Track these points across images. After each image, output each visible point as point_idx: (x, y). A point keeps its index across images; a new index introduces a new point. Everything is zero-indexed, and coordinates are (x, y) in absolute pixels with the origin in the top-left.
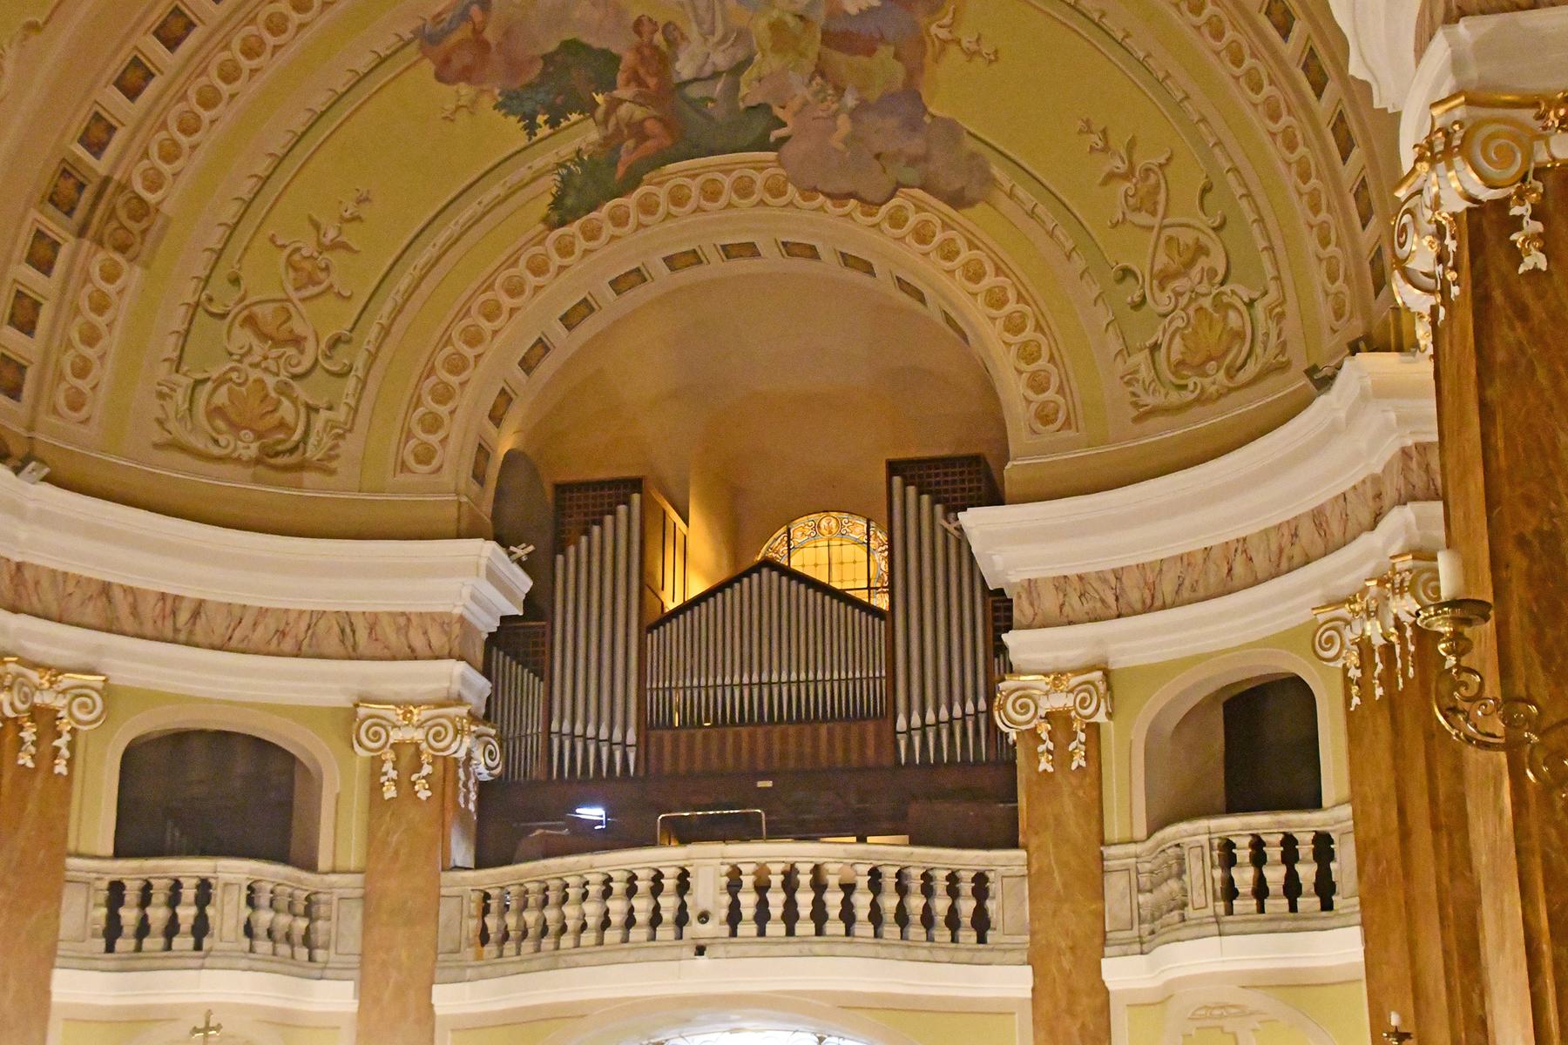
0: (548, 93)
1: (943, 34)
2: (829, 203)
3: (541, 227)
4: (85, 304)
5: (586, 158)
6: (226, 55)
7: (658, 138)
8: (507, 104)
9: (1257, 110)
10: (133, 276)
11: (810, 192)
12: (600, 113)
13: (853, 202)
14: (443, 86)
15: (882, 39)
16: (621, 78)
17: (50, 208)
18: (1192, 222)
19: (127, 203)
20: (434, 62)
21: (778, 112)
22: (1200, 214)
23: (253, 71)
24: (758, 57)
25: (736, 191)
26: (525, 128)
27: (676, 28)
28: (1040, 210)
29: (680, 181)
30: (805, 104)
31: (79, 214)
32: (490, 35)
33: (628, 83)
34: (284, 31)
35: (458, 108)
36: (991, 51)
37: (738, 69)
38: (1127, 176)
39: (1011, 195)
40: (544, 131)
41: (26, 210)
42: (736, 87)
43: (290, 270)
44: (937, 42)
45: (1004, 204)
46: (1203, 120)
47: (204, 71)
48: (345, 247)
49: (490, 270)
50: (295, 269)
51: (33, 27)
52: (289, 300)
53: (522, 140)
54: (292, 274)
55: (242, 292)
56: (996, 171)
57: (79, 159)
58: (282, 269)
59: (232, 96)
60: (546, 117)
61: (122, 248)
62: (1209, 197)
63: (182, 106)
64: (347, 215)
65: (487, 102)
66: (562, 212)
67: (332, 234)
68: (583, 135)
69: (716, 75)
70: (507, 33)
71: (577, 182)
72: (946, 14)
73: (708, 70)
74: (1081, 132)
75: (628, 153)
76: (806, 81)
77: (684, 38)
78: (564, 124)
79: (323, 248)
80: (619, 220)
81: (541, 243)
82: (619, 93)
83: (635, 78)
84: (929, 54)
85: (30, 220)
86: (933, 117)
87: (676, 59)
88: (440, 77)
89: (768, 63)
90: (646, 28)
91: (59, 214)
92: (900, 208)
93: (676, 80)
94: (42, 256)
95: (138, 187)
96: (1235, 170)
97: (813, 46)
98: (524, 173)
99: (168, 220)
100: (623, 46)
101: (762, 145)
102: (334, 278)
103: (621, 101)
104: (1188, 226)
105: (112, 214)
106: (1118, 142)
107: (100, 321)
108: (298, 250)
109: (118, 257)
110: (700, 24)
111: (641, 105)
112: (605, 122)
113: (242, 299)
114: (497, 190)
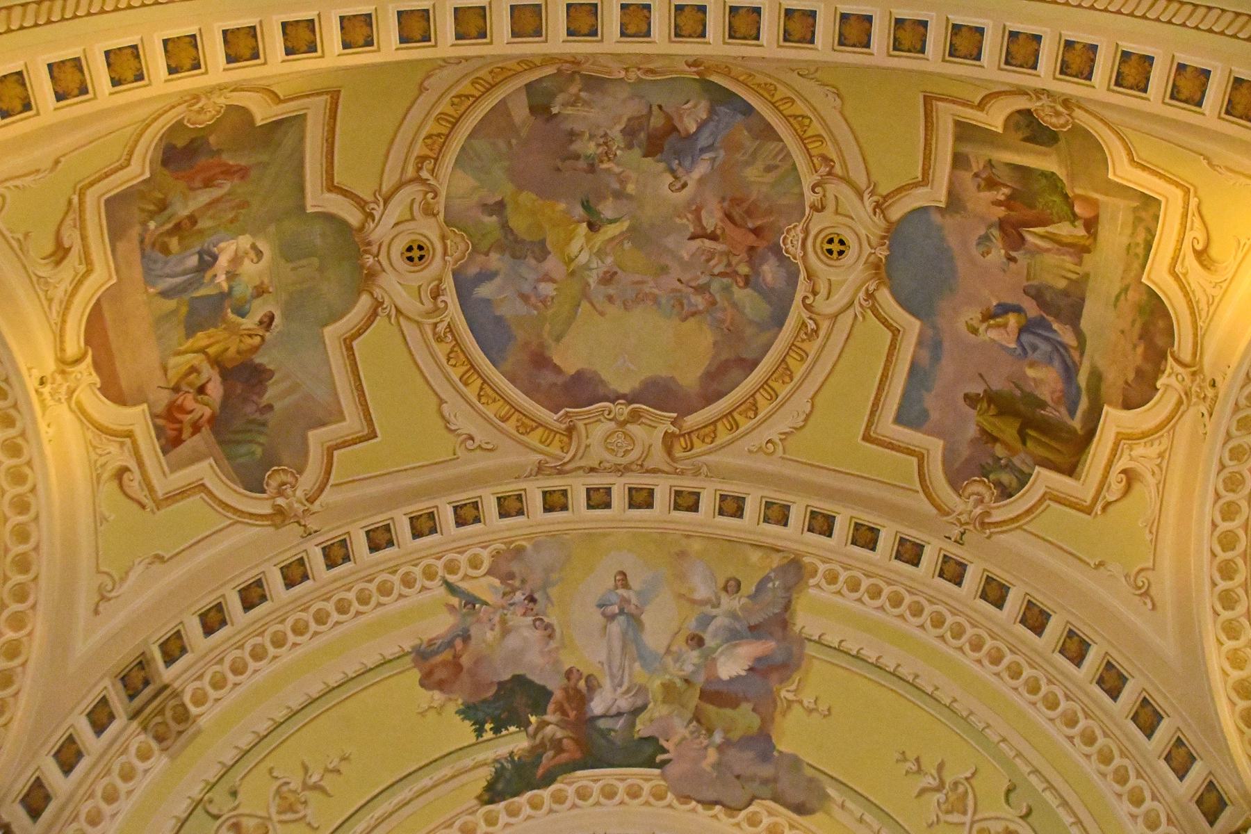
0: (496, 709)
1: (790, 696)
2: (700, 807)
3: (475, 802)
4: (116, 768)
5: (516, 758)
6: (280, 627)
7: (571, 750)
8: (468, 712)
9: (1054, 724)
10: (160, 762)
11: (685, 798)
12: (531, 729)
13: (718, 808)
14: (423, 690)
15: (746, 699)
16: (551, 707)
17: (120, 686)
18: (999, 814)
19: (175, 707)
20: (420, 671)
21: (662, 742)
22: (1006, 807)
23: (295, 645)
24: (651, 706)
25: (628, 794)
26: (475, 730)
27: (596, 678)
28: (867, 817)
29: (585, 783)
30: (684, 739)
31: (138, 702)
32: (465, 661)
33: (554, 712)
34: (324, 624)
35: (431, 707)
36: (826, 708)
37: (636, 712)
38: (940, 788)
39: (843, 806)
40: (489, 735)
41: (102, 678)
42: (633, 725)
43: (277, 798)
44: (784, 701)
45: (836, 811)
46: (1004, 740)
47: (261, 634)
48: (322, 790)
49: (453, 813)
50: (283, 798)
51: (160, 558)
52: (270, 819)
53: (474, 740)
54: (277, 800)
55: (237, 803)
56: (830, 791)
57: (153, 659)
58: (271, 795)
59: (275, 657)
60: (492, 725)
61: (160, 739)
62: (1012, 796)
63: (238, 653)
64: (331, 767)
65: (452, 708)
66: (493, 793)
67: (315, 778)
68: (516, 742)
69: (619, 714)
70: (476, 663)
71: (507, 775)
72: (793, 682)
73: (614, 711)
74: (898, 761)
75: (548, 758)
76: (685, 723)
77: (600, 686)
78: (504, 732)
79: (306, 786)
80: (535, 805)
81: (474, 813)
82: (548, 718)
83: (561, 709)
84: (779, 709)
85: (100, 687)
86: (780, 752)
87: (592, 699)
88: (422, 685)
89: (658, 710)
90: (575, 676)
91: (123, 694)
92: (755, 813)
93: (589, 715)
94: (100, 718)
95: (187, 699)
96: (1036, 771)
97: (693, 700)
98: (469, 762)
99: (199, 732)
100: (555, 685)
101: (650, 763)
102: (309, 811)
103: (548, 724)
104: (997, 818)
105: (161, 712)
106: (930, 766)
107: (123, 787)
108: (287, 783)
109: (154, 744)
110: (612, 676)
111: (562, 728)
112: (534, 736)
113: (235, 808)
114: (446, 771)
